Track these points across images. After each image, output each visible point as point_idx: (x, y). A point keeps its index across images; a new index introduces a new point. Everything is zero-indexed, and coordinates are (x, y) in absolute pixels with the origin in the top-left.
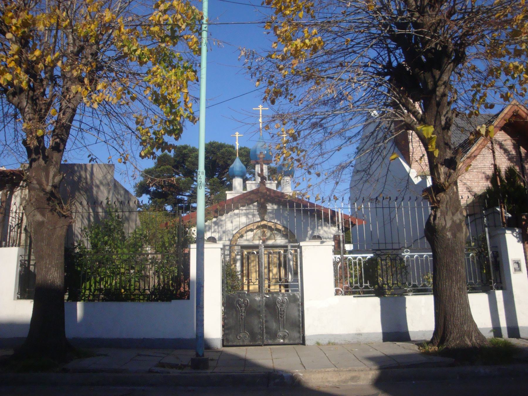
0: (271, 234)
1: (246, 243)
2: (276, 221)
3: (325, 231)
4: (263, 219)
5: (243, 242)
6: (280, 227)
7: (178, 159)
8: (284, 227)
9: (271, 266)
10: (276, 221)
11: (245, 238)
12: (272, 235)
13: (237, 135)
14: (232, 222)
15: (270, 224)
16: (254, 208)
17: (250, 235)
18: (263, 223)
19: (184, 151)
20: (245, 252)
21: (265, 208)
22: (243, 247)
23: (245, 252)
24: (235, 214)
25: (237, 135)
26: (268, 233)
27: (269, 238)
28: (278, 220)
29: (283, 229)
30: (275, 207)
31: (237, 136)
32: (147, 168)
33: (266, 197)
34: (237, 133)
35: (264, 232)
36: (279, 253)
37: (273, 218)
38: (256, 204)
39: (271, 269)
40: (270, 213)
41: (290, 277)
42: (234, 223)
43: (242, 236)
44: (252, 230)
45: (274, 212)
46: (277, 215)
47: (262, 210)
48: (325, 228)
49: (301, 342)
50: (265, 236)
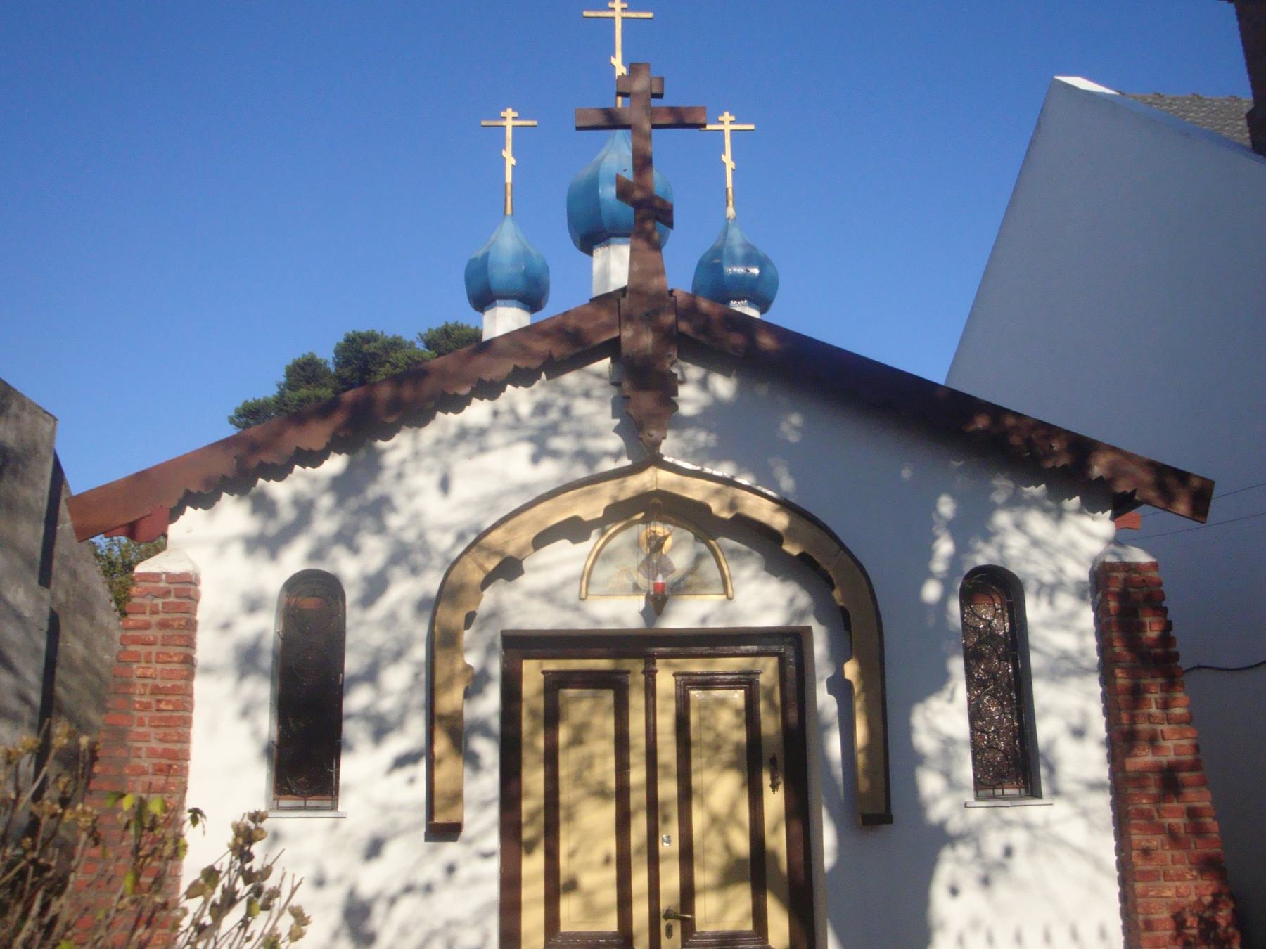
0: (699, 558)
1: (542, 618)
2: (724, 470)
3: (1036, 543)
4: (649, 458)
5: (526, 606)
6: (763, 510)
7: (346, 372)
8: (784, 504)
9: (695, 763)
10: (724, 470)
11: (529, 580)
12: (709, 565)
13: (510, 119)
14: (445, 485)
15: (696, 490)
16: (589, 398)
17: (564, 560)
18: (653, 479)
19: (369, 348)
20: (533, 673)
21: (667, 389)
22: (520, 645)
23: (533, 673)
24: (463, 434)
25: (510, 119)
26: (680, 551)
27: (681, 587)
28: (742, 466)
29: (780, 521)
30: (723, 386)
31: (509, 124)
32: (251, 400)
33: (669, 319)
34: (510, 113)
35: (656, 544)
36: (747, 681)
37: (717, 455)
38: (604, 364)
39: (696, 780)
40: (690, 422)
41: (829, 837)
42: (462, 488)
43: (510, 568)
44: (575, 530)
45: (713, 415)
46: (729, 432)
47: (645, 396)
48: (1038, 524)
49: (608, 697)
50: (665, 568)
